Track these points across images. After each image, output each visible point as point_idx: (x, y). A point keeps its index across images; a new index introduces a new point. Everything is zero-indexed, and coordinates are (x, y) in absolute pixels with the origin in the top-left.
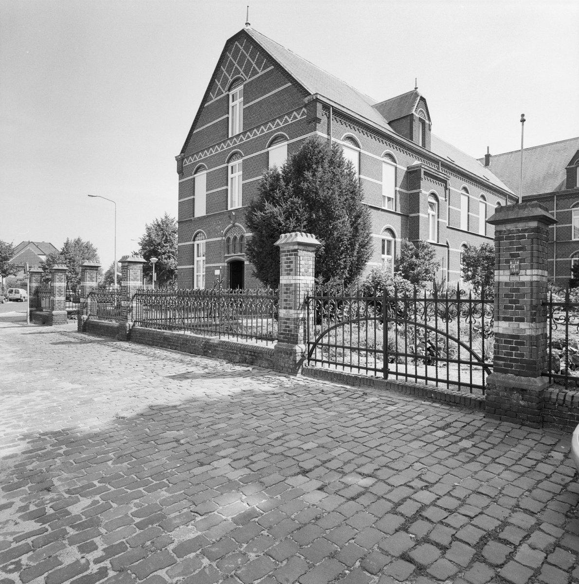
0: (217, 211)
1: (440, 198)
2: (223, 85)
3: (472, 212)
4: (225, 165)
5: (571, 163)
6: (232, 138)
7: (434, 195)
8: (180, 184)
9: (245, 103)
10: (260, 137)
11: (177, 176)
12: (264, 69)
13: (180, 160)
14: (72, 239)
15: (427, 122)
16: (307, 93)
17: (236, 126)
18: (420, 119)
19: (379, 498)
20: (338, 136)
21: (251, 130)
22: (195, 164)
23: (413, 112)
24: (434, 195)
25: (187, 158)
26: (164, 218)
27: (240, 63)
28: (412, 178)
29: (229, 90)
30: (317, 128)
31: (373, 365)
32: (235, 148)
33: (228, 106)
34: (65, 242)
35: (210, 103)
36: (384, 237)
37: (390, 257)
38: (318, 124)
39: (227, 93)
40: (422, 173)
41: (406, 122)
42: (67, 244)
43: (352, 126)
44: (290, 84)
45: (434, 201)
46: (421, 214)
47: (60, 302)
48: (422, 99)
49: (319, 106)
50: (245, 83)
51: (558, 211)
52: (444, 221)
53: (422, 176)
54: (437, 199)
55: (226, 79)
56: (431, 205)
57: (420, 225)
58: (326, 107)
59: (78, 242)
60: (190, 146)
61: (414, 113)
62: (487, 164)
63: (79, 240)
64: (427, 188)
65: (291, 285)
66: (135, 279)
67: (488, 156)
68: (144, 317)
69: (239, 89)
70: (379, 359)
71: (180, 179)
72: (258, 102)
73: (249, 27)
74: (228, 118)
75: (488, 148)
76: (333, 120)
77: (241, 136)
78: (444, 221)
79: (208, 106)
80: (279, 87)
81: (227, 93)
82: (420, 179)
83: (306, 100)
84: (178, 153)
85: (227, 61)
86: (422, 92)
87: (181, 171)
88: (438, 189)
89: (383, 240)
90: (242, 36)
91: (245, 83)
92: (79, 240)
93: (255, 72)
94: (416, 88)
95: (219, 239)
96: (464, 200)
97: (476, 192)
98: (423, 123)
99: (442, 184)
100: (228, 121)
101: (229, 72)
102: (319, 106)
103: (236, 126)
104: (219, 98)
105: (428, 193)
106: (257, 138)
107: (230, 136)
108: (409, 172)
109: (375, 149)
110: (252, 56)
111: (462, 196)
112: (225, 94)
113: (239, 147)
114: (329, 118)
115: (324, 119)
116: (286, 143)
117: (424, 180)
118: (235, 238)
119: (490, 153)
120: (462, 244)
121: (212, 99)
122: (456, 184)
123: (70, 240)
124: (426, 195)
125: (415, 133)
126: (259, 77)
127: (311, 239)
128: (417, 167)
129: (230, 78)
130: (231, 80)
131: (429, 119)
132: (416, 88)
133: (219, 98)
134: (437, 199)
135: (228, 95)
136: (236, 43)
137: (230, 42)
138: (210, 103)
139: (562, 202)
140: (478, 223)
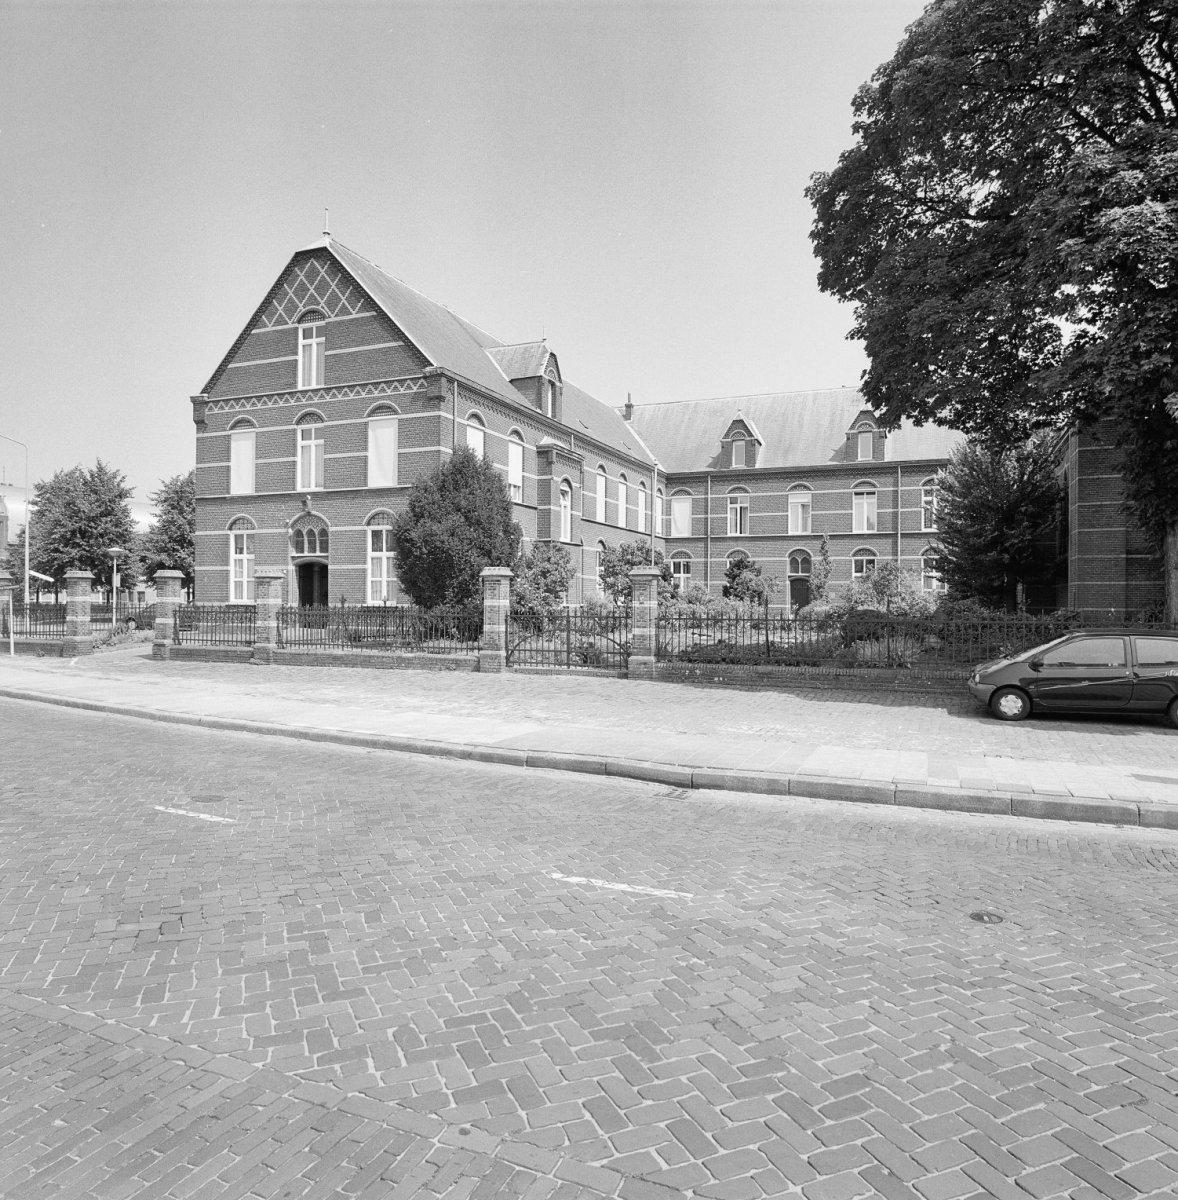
0: (277, 490)
1: (573, 484)
7: (566, 480)
8: (257, 466)
15: (558, 384)
18: (550, 381)
24: (566, 480)
26: (95, 470)
39: (297, 325)
40: (554, 455)
45: (568, 489)
47: (83, 623)
48: (552, 355)
52: (578, 514)
53: (554, 459)
54: (570, 487)
56: (564, 493)
58: (451, 380)
60: (221, 386)
65: (495, 607)
66: (276, 597)
75: (629, 395)
78: (578, 514)
79: (258, 334)
85: (295, 280)
88: (570, 473)
95: (283, 530)
96: (601, 482)
97: (614, 468)
98: (553, 384)
105: (560, 480)
109: (502, 426)
111: (598, 477)
118: (311, 533)
120: (598, 539)
121: (265, 326)
122: (591, 462)
129: (301, 305)
131: (560, 380)
134: (570, 487)
137: (301, 257)
140: (617, 511)
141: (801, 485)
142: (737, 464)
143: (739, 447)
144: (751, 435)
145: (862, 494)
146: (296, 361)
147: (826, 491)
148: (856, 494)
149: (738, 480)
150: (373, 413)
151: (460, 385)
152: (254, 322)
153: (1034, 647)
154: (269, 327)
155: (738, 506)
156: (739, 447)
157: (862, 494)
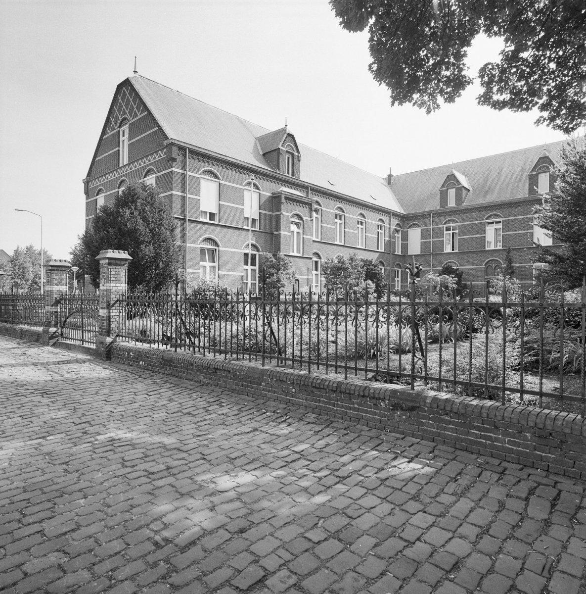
1: (304, 218)
2: (116, 122)
3: (349, 228)
4: (116, 190)
5: (443, 186)
6: (121, 167)
8: (87, 203)
9: (130, 139)
10: (139, 169)
11: (84, 196)
12: (141, 113)
13: (87, 183)
14: (23, 247)
15: (296, 154)
16: (166, 138)
17: (124, 159)
19: (385, 498)
20: (196, 170)
21: (133, 163)
22: (96, 187)
23: (280, 147)
25: (91, 181)
27: (127, 105)
28: (274, 203)
29: (120, 127)
30: (174, 165)
31: (538, 386)
32: (123, 176)
33: (119, 141)
34: (16, 249)
35: (107, 136)
36: (247, 252)
37: (253, 268)
38: (174, 163)
41: (275, 154)
42: (17, 252)
43: (210, 162)
44: (157, 128)
46: (282, 232)
48: (291, 136)
49: (175, 149)
50: (129, 123)
51: (433, 227)
53: (283, 200)
55: (117, 118)
57: (281, 241)
58: (182, 149)
59: (30, 249)
60: (93, 172)
61: (281, 148)
62: (389, 183)
63: (31, 247)
64: (287, 212)
66: (118, 281)
67: (390, 176)
68: (289, 326)
69: (125, 128)
70: (464, 369)
71: (87, 199)
72: (138, 140)
73: (136, 75)
74: (119, 150)
76: (189, 158)
77: (127, 167)
80: (151, 129)
81: (118, 129)
82: (280, 203)
83: (165, 143)
84: (85, 177)
86: (290, 130)
87: (87, 192)
89: (246, 255)
90: (127, 83)
91: (129, 123)
92: (31, 247)
93: (136, 115)
94: (286, 126)
99: (307, 206)
100: (119, 153)
101: (119, 112)
102: (175, 149)
103: (124, 159)
104: (113, 132)
106: (137, 170)
107: (120, 166)
108: (275, 197)
110: (134, 101)
112: (117, 130)
113: (102, 185)
114: (185, 157)
115: (180, 159)
116: (155, 175)
117: (285, 204)
119: (392, 173)
121: (108, 133)
123: (20, 247)
124: (287, 216)
125: (281, 164)
126: (138, 120)
127: (124, 255)
128: (279, 193)
129: (120, 117)
130: (120, 119)
131: (298, 151)
132: (286, 126)
133: (113, 132)
134: (301, 219)
135: (119, 131)
136: (124, 88)
137: (120, 87)
138: (107, 136)
139: (437, 219)
141: (453, 220)
142: (452, 203)
143: (452, 193)
144: (459, 183)
145: (493, 223)
146: (443, 240)
147: (513, 218)
148: (489, 223)
149: (451, 215)
150: (409, 228)
151: (312, 189)
152: (104, 132)
153: (129, 150)
154: (110, 133)
155: (451, 232)
156: (452, 193)
157: (493, 223)
